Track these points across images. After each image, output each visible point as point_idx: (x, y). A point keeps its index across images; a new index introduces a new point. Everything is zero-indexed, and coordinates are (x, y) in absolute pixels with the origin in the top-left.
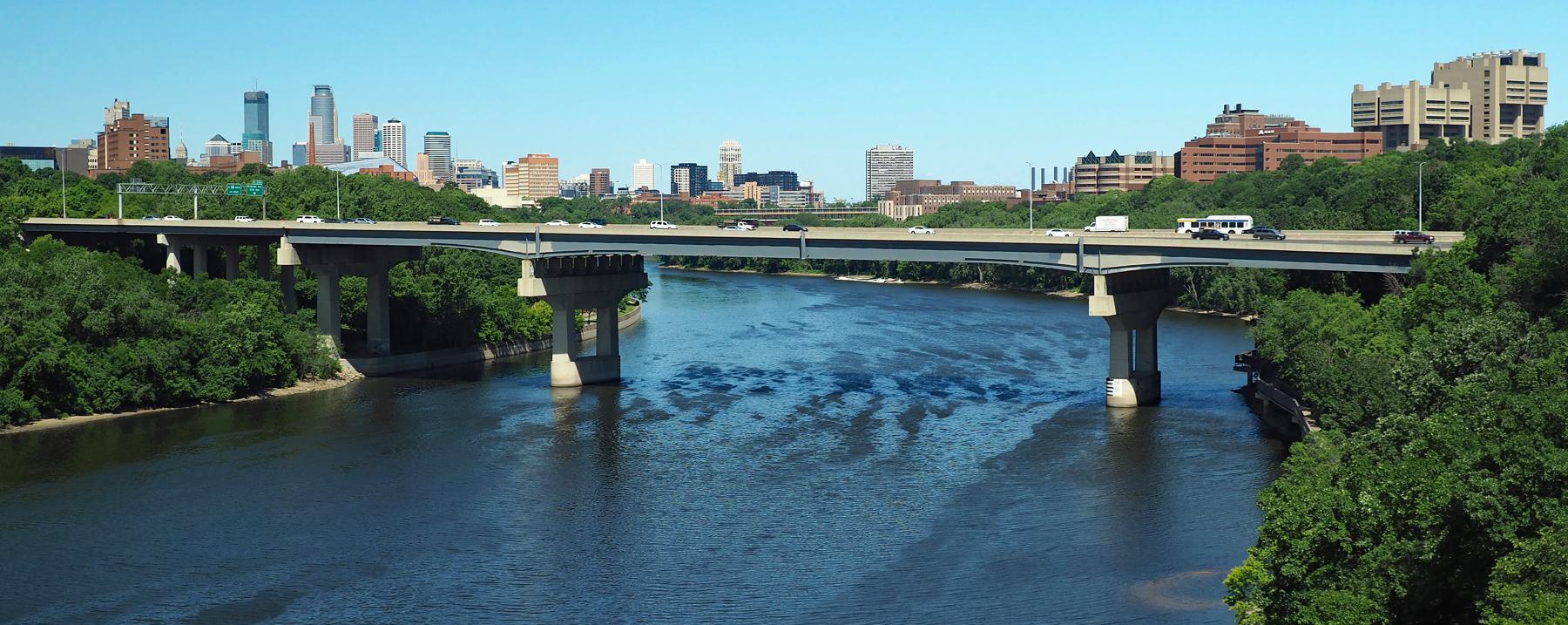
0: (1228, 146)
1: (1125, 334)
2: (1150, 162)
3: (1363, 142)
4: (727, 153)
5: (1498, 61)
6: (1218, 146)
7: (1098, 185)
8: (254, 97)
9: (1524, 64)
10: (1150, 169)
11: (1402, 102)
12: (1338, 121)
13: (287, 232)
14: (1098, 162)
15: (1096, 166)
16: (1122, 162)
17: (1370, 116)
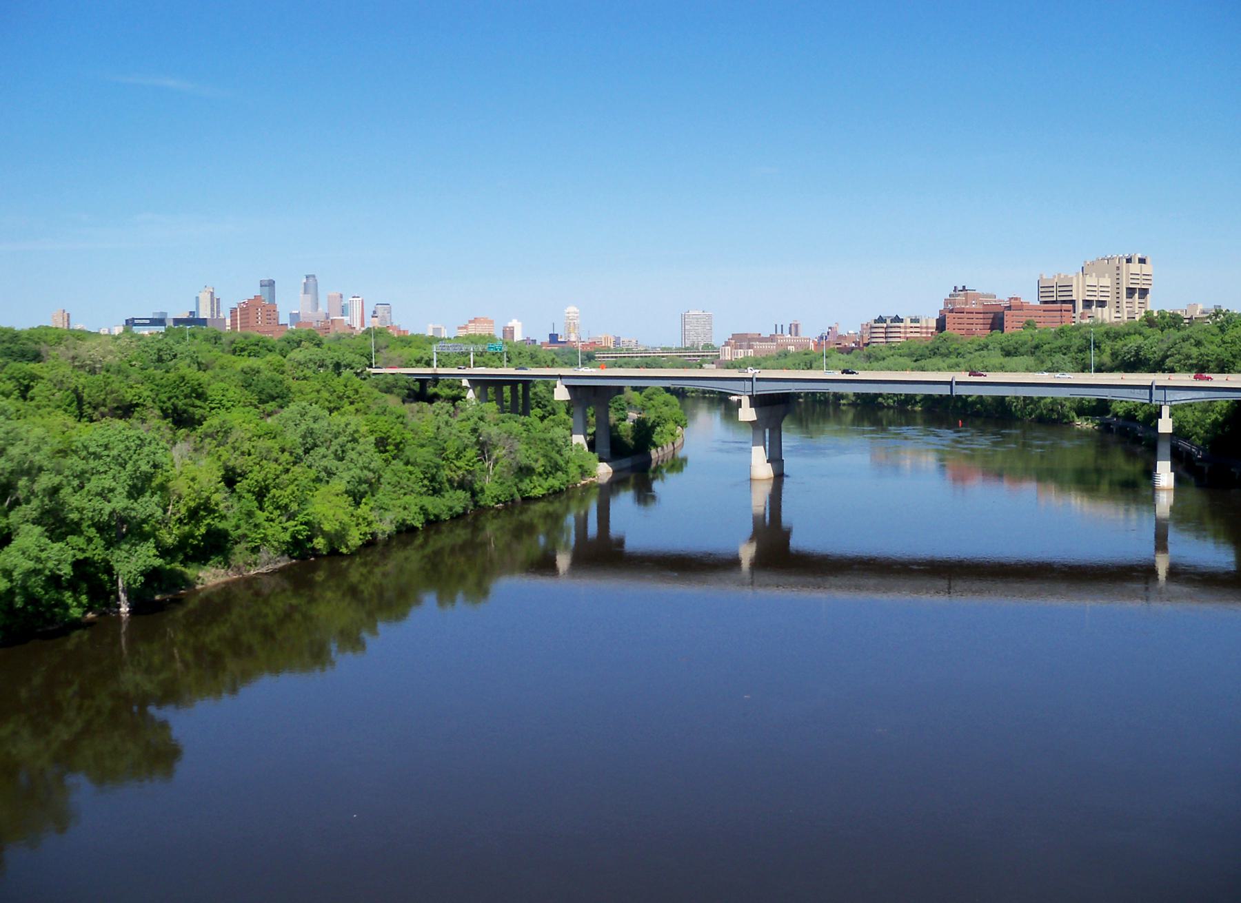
0: (973, 313)
1: (761, 432)
2: (919, 322)
3: (1061, 310)
4: (570, 315)
5: (1125, 260)
6: (967, 313)
7: (886, 337)
8: (266, 283)
9: (1139, 263)
10: (918, 327)
11: (1072, 286)
12: (1031, 298)
13: (561, 377)
14: (885, 322)
15: (885, 325)
16: (902, 322)
17: (1051, 294)
